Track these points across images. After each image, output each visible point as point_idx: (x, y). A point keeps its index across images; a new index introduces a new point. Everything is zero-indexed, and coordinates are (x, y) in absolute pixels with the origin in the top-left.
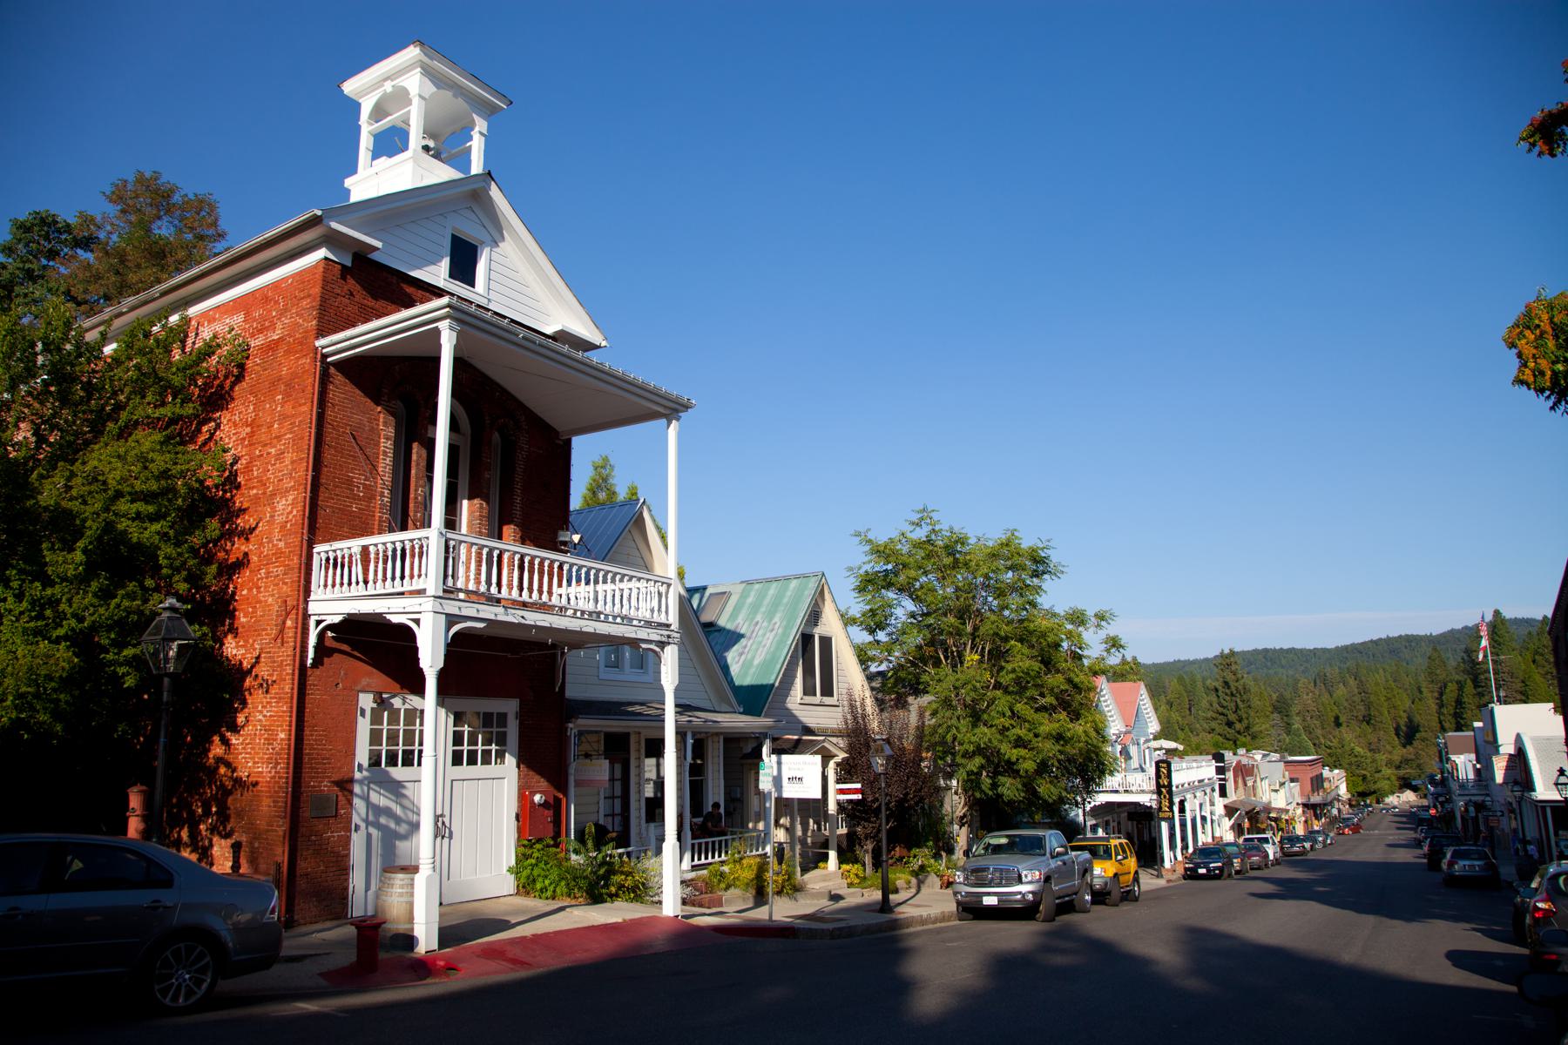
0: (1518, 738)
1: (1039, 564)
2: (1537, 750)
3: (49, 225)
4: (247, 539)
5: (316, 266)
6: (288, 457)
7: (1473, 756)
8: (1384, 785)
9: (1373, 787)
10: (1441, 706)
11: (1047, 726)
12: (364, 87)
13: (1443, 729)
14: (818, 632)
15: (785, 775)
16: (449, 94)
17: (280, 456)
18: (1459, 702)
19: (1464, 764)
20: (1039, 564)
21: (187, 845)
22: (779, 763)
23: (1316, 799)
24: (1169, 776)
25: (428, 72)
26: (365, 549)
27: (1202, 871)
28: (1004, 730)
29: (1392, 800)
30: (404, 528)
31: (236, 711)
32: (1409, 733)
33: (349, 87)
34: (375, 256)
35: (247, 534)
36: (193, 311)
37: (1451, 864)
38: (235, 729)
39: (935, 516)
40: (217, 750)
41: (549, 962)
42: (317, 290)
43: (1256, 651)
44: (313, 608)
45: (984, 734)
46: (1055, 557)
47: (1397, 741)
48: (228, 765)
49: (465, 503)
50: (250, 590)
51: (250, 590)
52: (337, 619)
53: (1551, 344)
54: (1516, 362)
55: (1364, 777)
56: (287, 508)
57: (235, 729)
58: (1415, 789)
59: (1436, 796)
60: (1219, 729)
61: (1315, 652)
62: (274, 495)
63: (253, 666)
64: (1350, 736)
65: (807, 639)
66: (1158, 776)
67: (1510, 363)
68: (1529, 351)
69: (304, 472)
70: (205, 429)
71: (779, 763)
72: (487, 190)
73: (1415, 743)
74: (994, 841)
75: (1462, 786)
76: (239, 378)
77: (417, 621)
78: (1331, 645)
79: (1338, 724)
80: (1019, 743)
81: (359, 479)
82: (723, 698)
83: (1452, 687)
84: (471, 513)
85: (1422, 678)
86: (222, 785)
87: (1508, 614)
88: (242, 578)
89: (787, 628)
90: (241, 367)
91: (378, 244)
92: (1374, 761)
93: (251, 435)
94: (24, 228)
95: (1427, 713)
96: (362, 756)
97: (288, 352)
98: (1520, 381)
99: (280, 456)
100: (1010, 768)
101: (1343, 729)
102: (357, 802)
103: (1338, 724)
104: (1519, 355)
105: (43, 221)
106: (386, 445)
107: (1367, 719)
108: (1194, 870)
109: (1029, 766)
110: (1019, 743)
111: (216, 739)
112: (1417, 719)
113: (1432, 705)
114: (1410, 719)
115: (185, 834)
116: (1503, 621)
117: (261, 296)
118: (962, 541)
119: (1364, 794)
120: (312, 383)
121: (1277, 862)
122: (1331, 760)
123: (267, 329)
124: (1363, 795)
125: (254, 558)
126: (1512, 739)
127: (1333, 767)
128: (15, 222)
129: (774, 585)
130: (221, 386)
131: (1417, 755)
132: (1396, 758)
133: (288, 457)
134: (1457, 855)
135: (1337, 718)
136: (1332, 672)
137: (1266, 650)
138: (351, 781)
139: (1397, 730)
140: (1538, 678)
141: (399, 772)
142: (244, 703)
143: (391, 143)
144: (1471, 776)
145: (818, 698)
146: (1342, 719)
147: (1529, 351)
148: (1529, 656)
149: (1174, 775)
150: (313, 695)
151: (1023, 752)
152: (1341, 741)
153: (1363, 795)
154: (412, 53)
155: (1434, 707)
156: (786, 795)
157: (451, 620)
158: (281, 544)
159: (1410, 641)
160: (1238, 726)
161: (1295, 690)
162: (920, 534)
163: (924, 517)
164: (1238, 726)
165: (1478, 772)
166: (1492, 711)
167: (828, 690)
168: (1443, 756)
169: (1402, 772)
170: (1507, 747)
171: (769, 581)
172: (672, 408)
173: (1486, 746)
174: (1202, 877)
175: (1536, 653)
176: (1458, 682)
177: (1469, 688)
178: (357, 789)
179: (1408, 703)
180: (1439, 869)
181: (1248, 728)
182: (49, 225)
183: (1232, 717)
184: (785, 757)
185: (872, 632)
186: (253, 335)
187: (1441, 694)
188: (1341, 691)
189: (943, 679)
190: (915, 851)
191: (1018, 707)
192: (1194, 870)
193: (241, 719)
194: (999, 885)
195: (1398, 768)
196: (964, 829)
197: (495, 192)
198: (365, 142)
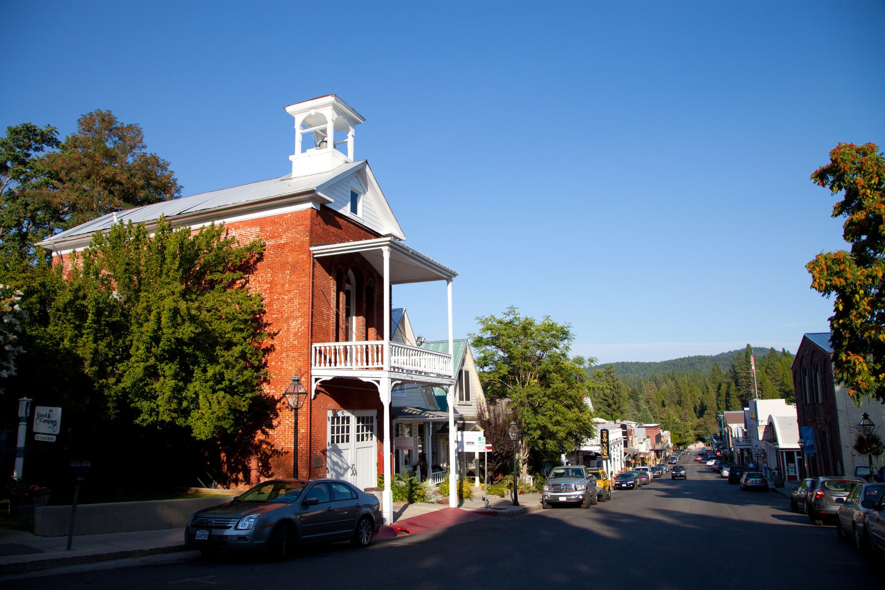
0: (770, 417)
1: (564, 334)
2: (780, 423)
3: (31, 131)
4: (273, 338)
5: (306, 210)
6: (296, 302)
7: (743, 425)
8: (690, 439)
9: (684, 440)
10: (718, 395)
11: (571, 415)
12: (299, 111)
14: (465, 368)
15: (465, 441)
16: (341, 117)
17: (291, 300)
18: (728, 394)
19: (736, 429)
20: (564, 334)
21: (242, 481)
22: (462, 435)
23: (658, 447)
24: (607, 437)
25: (336, 108)
26: (345, 347)
27: (624, 485)
28: (551, 417)
29: (692, 447)
30: (367, 339)
31: (272, 419)
32: (701, 411)
33: (289, 109)
34: (329, 205)
35: (272, 336)
36: (228, 220)
37: (746, 480)
38: (272, 427)
39: (517, 311)
40: (259, 436)
41: (437, 529)
42: (308, 222)
43: (618, 363)
44: (314, 372)
45: (542, 420)
46: (572, 331)
47: (694, 415)
48: (268, 444)
49: (354, 318)
50: (276, 362)
51: (276, 362)
52: (329, 378)
53: (825, 273)
54: (811, 280)
55: (680, 435)
56: (298, 325)
57: (272, 427)
58: (703, 441)
59: (718, 445)
60: (603, 408)
61: (649, 364)
62: (288, 318)
63: (281, 399)
64: (672, 412)
65: (460, 372)
66: (602, 438)
67: (809, 279)
68: (817, 275)
69: (307, 309)
70: (238, 282)
71: (462, 435)
72: (364, 169)
73: (705, 416)
74: (557, 471)
75: (737, 440)
76: (261, 258)
77: (378, 382)
78: (658, 361)
79: (664, 405)
80: (558, 423)
81: (325, 311)
82: (431, 404)
83: (724, 386)
84: (357, 323)
85: (707, 380)
86: (265, 453)
87: (753, 346)
88: (271, 358)
89: (455, 367)
90: (261, 254)
91: (332, 200)
92: (685, 426)
93: (271, 288)
94: (14, 132)
95: (711, 400)
96: (329, 440)
97: (291, 250)
98: (812, 287)
99: (291, 300)
100: (552, 435)
101: (667, 408)
102: (328, 460)
103: (664, 405)
104: (813, 277)
105: (28, 129)
106: (333, 294)
107: (679, 403)
108: (620, 485)
109: (562, 434)
110: (558, 423)
111: (259, 432)
112: (706, 403)
113: (713, 394)
114: (702, 403)
115: (241, 476)
116: (751, 349)
117: (273, 221)
118: (531, 324)
119: (680, 444)
120: (308, 267)
121: (652, 481)
122: (663, 426)
123: (277, 237)
124: (679, 444)
125: (278, 348)
127: (665, 429)
128: (10, 129)
129: (441, 345)
130: (248, 262)
131: (705, 422)
132: (695, 424)
133: (296, 302)
134: (749, 476)
135: (663, 402)
136: (660, 376)
137: (623, 363)
138: (326, 450)
139: (695, 408)
140: (768, 381)
141: (341, 446)
142: (277, 415)
143: (315, 140)
144: (741, 435)
145: (464, 402)
146: (666, 403)
147: (817, 275)
148: (764, 368)
149: (610, 436)
150: (314, 412)
151: (559, 428)
152: (668, 415)
153: (679, 444)
154: (330, 99)
155: (715, 397)
156: (465, 450)
157: (393, 380)
158: (295, 342)
159: (701, 359)
160: (614, 407)
161: (641, 386)
162: (507, 319)
163: (512, 310)
164: (614, 407)
165: (745, 434)
167: (468, 399)
168: (721, 423)
169: (697, 432)
170: (763, 422)
171: (438, 342)
172: (448, 276)
173: (751, 422)
174: (625, 488)
175: (767, 368)
176: (728, 383)
177: (733, 386)
178: (328, 454)
179: (701, 395)
180: (738, 483)
181: (619, 408)
182: (31, 131)
183: (611, 402)
184: (465, 432)
185: (482, 367)
186: (267, 239)
187: (719, 389)
188: (664, 387)
189: (518, 392)
190: (507, 476)
191: (556, 405)
192: (620, 485)
193: (275, 423)
194: (566, 491)
195: (695, 429)
196: (526, 465)
197: (368, 170)
198: (298, 138)
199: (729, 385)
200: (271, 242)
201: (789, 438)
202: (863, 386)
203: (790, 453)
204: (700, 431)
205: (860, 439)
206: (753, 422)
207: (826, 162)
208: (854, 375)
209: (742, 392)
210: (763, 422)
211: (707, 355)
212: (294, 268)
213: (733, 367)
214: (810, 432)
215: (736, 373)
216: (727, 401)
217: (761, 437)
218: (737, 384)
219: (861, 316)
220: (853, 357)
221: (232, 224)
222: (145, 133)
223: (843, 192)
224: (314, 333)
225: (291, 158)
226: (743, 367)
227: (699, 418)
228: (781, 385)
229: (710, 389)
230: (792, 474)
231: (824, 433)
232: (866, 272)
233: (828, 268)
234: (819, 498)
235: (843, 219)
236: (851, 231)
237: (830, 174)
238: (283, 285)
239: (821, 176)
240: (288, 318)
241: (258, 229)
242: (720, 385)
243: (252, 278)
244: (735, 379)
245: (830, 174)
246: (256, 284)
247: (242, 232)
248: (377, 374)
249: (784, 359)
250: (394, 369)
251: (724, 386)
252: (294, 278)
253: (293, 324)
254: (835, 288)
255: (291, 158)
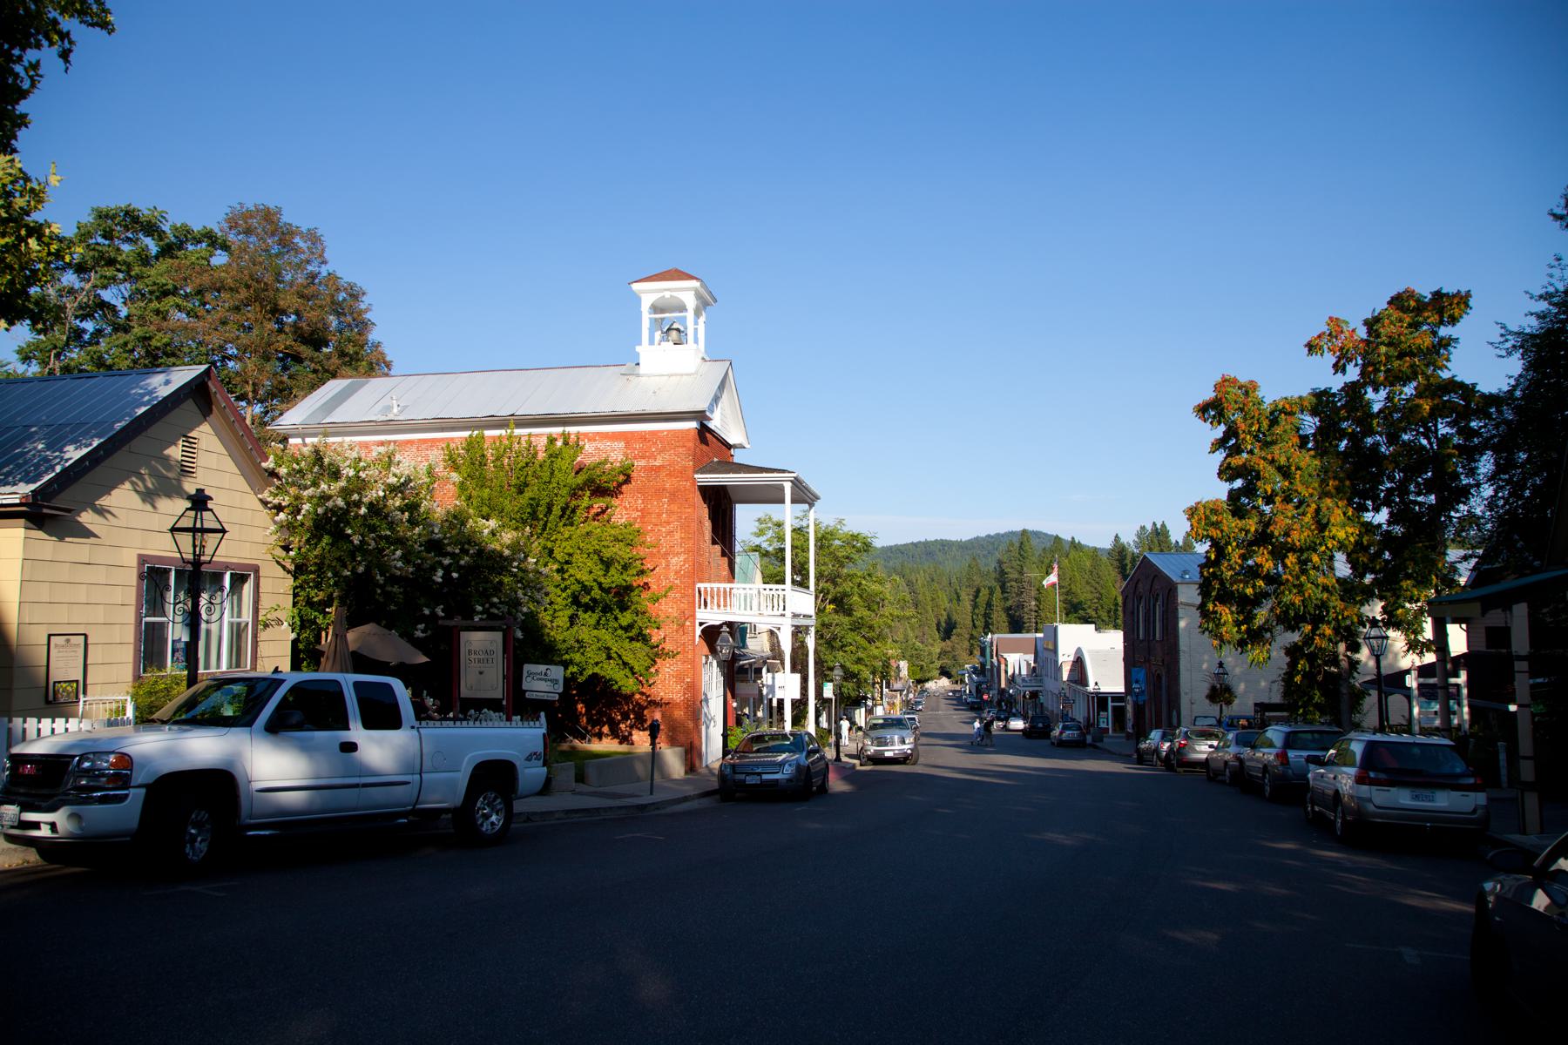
6: (677, 536)
7: (1031, 658)
10: (975, 606)
12: (650, 293)
13: (987, 628)
18: (989, 605)
19: (1017, 662)
32: (948, 630)
42: (691, 444)
48: (642, 694)
58: (949, 676)
76: (628, 480)
83: (984, 592)
94: (102, 216)
95: (964, 614)
97: (670, 475)
99: (670, 533)
112: (955, 617)
114: (949, 617)
115: (606, 729)
117: (643, 437)
126: (1072, 652)
133: (677, 536)
134: (1065, 728)
144: (1024, 672)
155: (969, 608)
159: (944, 545)
166: (1056, 629)
173: (1046, 654)
177: (998, 593)
187: (976, 597)
198: (646, 324)
199: (991, 593)
200: (642, 463)
201: (1108, 677)
202: (1227, 637)
203: (1101, 700)
204: (946, 661)
205: (1213, 688)
206: (1050, 655)
207: (1209, 395)
208: (1218, 626)
209: (1009, 603)
210: (1065, 656)
211: (953, 539)
212: (673, 496)
213: (1000, 562)
214: (1140, 674)
215: (1003, 573)
216: (987, 616)
217: (1065, 678)
218: (1003, 588)
219: (1231, 568)
220: (1219, 608)
221: (586, 434)
222: (328, 241)
223: (1222, 428)
224: (698, 572)
225: (638, 349)
226: (1014, 564)
227: (943, 640)
228: (1067, 593)
229: (963, 596)
230: (1103, 725)
231: (1159, 677)
232: (1241, 523)
233: (1207, 517)
234: (1182, 747)
235: (1220, 456)
236: (1227, 473)
237: (1211, 410)
238: (659, 515)
239: (1203, 410)
240: (667, 554)
241: (622, 444)
242: (978, 591)
243: (615, 502)
244: (1007, 583)
245: (1211, 410)
246: (622, 512)
247: (601, 449)
248: (779, 620)
249: (1073, 554)
250: (795, 616)
251: (984, 592)
252: (674, 507)
253: (674, 560)
254: (1212, 539)
255: (638, 349)
